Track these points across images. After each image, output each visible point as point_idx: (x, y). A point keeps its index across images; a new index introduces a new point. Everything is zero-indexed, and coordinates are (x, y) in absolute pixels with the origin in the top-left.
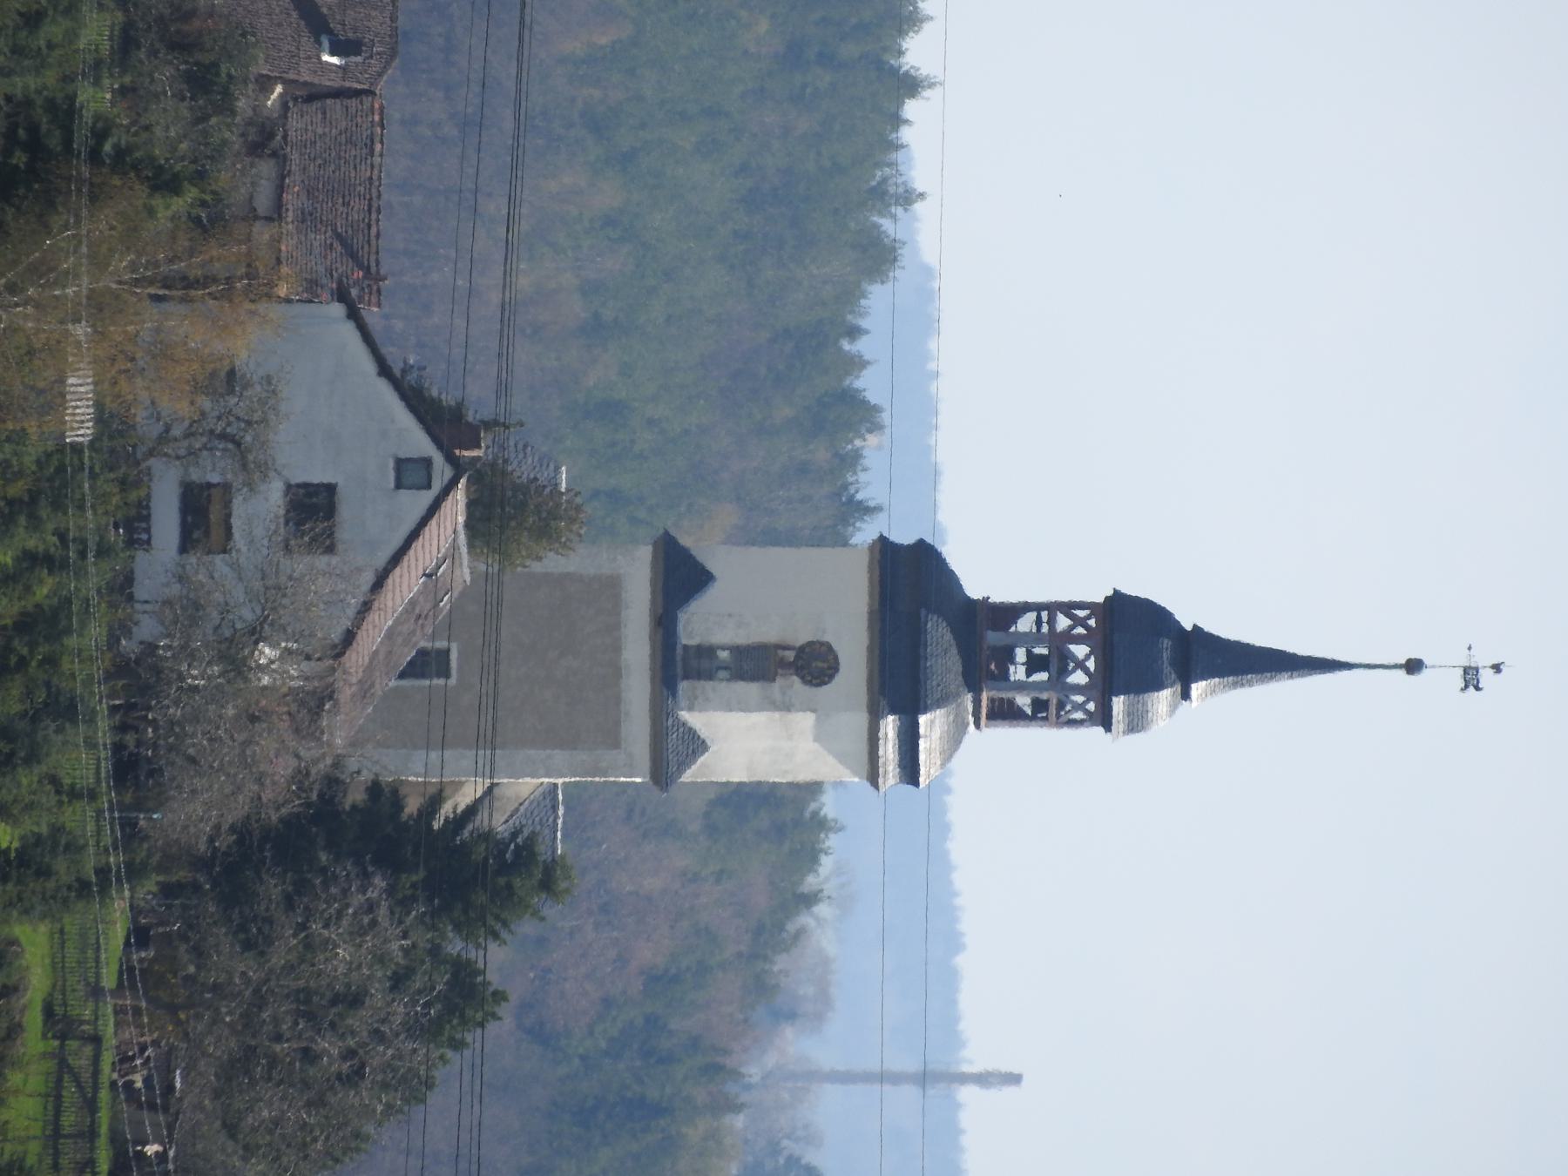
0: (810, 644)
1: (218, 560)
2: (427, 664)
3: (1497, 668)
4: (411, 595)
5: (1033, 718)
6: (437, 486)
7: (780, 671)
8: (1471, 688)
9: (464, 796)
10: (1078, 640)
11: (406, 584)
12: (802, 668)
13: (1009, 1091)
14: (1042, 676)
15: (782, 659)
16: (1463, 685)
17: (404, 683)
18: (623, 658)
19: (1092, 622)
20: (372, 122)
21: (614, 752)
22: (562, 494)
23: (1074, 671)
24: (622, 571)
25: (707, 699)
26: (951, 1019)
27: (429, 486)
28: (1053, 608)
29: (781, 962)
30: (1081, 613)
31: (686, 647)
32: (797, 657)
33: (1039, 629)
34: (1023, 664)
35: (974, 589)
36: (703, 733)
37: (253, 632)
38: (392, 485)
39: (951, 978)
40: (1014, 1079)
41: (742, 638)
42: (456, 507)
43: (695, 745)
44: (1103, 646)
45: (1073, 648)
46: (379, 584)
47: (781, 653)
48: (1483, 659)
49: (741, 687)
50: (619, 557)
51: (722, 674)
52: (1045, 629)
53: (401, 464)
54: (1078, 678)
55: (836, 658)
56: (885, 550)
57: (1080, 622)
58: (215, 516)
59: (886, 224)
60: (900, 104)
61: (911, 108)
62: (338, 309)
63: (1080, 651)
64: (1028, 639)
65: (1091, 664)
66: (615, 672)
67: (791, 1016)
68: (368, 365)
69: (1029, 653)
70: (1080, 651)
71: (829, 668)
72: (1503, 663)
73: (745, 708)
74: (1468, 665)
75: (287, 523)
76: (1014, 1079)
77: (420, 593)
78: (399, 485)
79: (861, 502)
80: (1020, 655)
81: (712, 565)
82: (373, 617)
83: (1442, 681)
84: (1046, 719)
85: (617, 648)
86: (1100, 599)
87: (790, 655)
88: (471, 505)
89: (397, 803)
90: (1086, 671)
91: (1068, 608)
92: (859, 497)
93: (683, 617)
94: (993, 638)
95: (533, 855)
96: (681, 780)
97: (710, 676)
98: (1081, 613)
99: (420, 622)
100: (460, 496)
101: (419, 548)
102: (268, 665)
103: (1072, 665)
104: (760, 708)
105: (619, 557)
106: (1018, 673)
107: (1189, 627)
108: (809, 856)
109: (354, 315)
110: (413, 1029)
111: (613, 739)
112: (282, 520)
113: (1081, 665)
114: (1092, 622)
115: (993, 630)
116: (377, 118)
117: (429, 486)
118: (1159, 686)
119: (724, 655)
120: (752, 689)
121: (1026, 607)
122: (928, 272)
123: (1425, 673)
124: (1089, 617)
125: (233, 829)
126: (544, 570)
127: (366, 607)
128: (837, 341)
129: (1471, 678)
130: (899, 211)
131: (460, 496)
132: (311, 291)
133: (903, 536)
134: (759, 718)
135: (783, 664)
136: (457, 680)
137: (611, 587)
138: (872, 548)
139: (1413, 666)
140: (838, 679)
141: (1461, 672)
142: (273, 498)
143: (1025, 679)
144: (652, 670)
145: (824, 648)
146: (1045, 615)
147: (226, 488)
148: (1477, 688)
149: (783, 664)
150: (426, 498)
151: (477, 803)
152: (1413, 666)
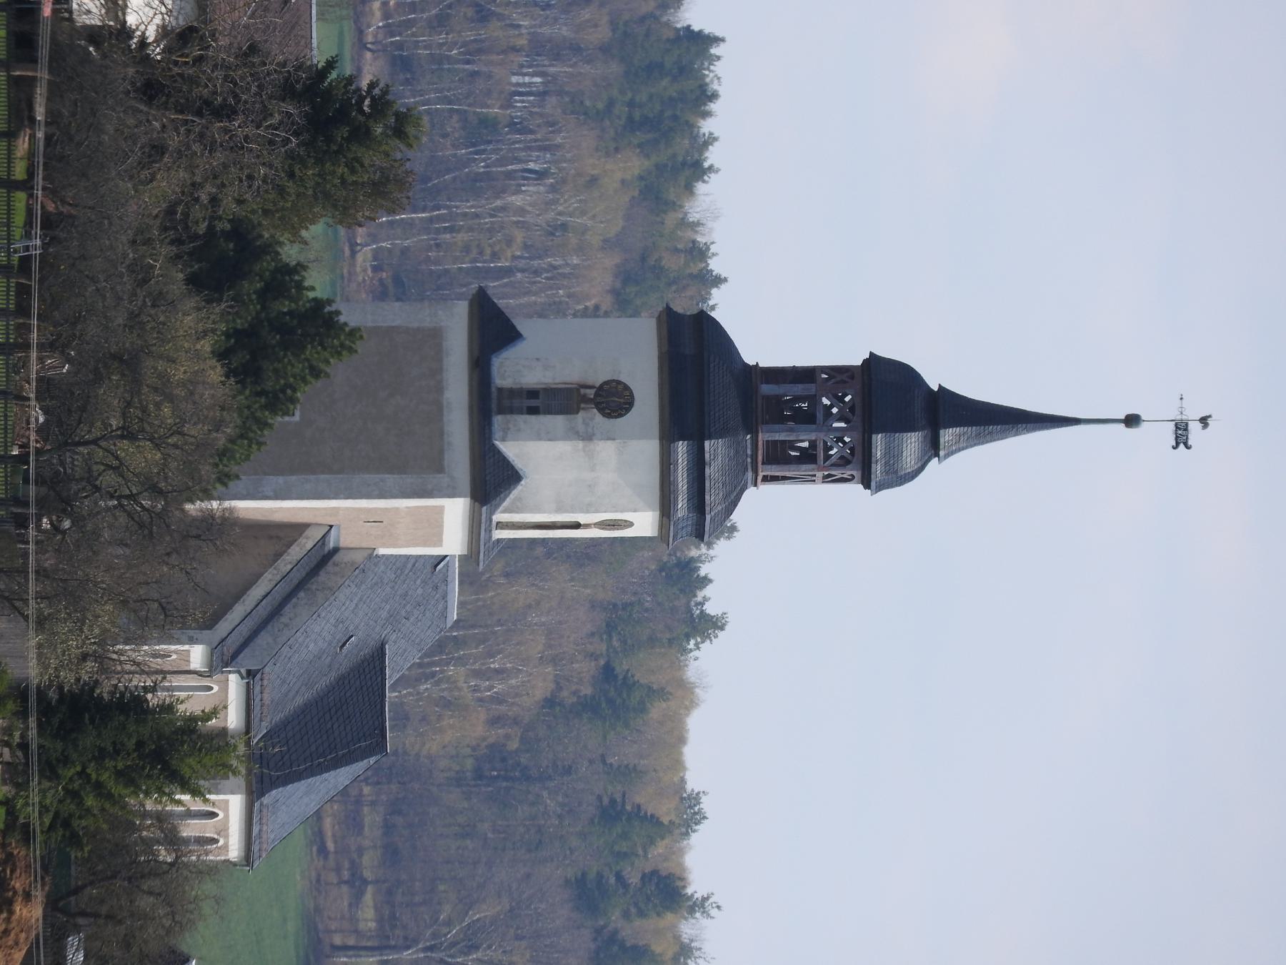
3: (1204, 421)
7: (582, 405)
8: (1182, 446)
9: (307, 538)
15: (585, 395)
16: (1175, 444)
18: (445, 397)
24: (442, 324)
25: (519, 430)
31: (500, 390)
32: (596, 394)
35: (749, 357)
36: (518, 463)
47: (583, 391)
48: (1192, 414)
50: (440, 312)
66: (437, 412)
71: (625, 404)
72: (1210, 416)
73: (552, 438)
74: (1179, 417)
81: (521, 325)
83: (1158, 435)
85: (440, 389)
86: (859, 363)
87: (591, 393)
95: (389, 104)
104: (566, 438)
105: (440, 312)
107: (936, 388)
118: (912, 429)
123: (1144, 425)
126: (374, 325)
129: (1181, 435)
134: (564, 447)
135: (585, 399)
136: (300, 417)
137: (435, 336)
139: (1132, 421)
141: (1172, 425)
144: (471, 408)
145: (620, 387)
148: (1188, 447)
149: (585, 399)
152: (1132, 421)
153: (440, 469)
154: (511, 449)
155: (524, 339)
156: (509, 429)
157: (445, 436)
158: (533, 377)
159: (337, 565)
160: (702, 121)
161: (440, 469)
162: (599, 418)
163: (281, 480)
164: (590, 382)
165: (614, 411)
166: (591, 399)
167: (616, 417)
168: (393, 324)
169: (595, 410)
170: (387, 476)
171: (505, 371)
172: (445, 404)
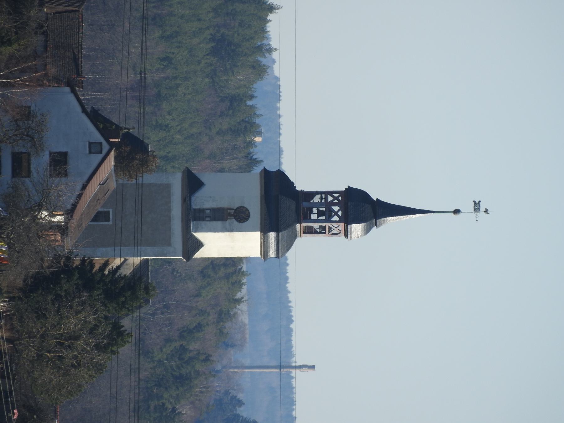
0: (239, 208)
1: (27, 180)
2: (101, 216)
4: (95, 192)
5: (320, 233)
6: (104, 151)
7: (229, 217)
10: (335, 205)
11: (93, 188)
12: (236, 216)
13: (311, 371)
14: (323, 218)
15: (230, 213)
17: (92, 223)
18: (172, 213)
19: (340, 198)
20: (79, 21)
21: (169, 247)
22: (150, 152)
23: (334, 215)
26: (289, 348)
27: (101, 152)
28: (327, 193)
29: (228, 324)
30: (336, 195)
31: (195, 210)
32: (235, 212)
33: (321, 200)
34: (316, 214)
35: (298, 188)
37: (39, 205)
38: (88, 152)
39: (289, 332)
40: (313, 367)
41: (213, 205)
42: (111, 161)
43: (199, 245)
44: (344, 206)
45: (334, 208)
46: (84, 187)
47: (229, 211)
49: (215, 223)
51: (207, 219)
52: (323, 201)
53: (90, 144)
54: (336, 218)
55: (249, 213)
56: (266, 173)
57: (335, 198)
58: (25, 164)
59: (261, 59)
60: (267, 15)
61: (271, 16)
62: (67, 89)
63: (336, 208)
64: (318, 205)
65: (340, 213)
66: (169, 219)
67: (233, 346)
68: (79, 109)
69: (318, 210)
70: (336, 208)
74: (478, 213)
75: (50, 166)
76: (313, 367)
77: (98, 191)
78: (90, 152)
79: (256, 159)
80: (315, 210)
82: (83, 199)
84: (325, 233)
85: (169, 210)
86: (344, 190)
87: (232, 212)
88: (116, 158)
89: (92, 265)
90: (338, 216)
91: (331, 193)
92: (254, 157)
93: (193, 198)
94: (305, 204)
96: (194, 257)
97: (203, 219)
98: (336, 195)
99: (99, 201)
100: (112, 154)
101: (106, 164)
102: (44, 217)
103: (333, 214)
106: (314, 217)
107: (375, 200)
108: (239, 285)
109: (73, 91)
110: (98, 347)
111: (168, 242)
112: (48, 165)
113: (336, 214)
114: (340, 198)
115: (305, 202)
116: (80, 20)
117: (101, 152)
119: (208, 211)
120: (219, 224)
121: (317, 193)
122: (277, 79)
124: (339, 197)
125: (32, 277)
127: (80, 196)
128: (245, 101)
130: (267, 55)
131: (112, 154)
132: (57, 80)
133: (272, 168)
135: (230, 215)
137: (168, 187)
138: (261, 172)
139: (457, 212)
140: (250, 219)
142: (46, 158)
143: (317, 219)
145: (245, 209)
146: (323, 196)
147: (29, 155)
149: (230, 215)
150: (100, 156)
151: (122, 264)
152: (457, 212)
153: (170, 245)
154: (199, 235)
155: (205, 185)
156: (198, 227)
157: (172, 230)
158: (208, 205)
159: (128, 265)
160: (269, 14)
161: (170, 245)
162: (235, 222)
163: (104, 249)
164: (232, 207)
165: (242, 220)
166: (232, 215)
167: (242, 222)
168: (150, 182)
169: (234, 219)
170: (148, 247)
171: (197, 202)
172: (172, 216)
